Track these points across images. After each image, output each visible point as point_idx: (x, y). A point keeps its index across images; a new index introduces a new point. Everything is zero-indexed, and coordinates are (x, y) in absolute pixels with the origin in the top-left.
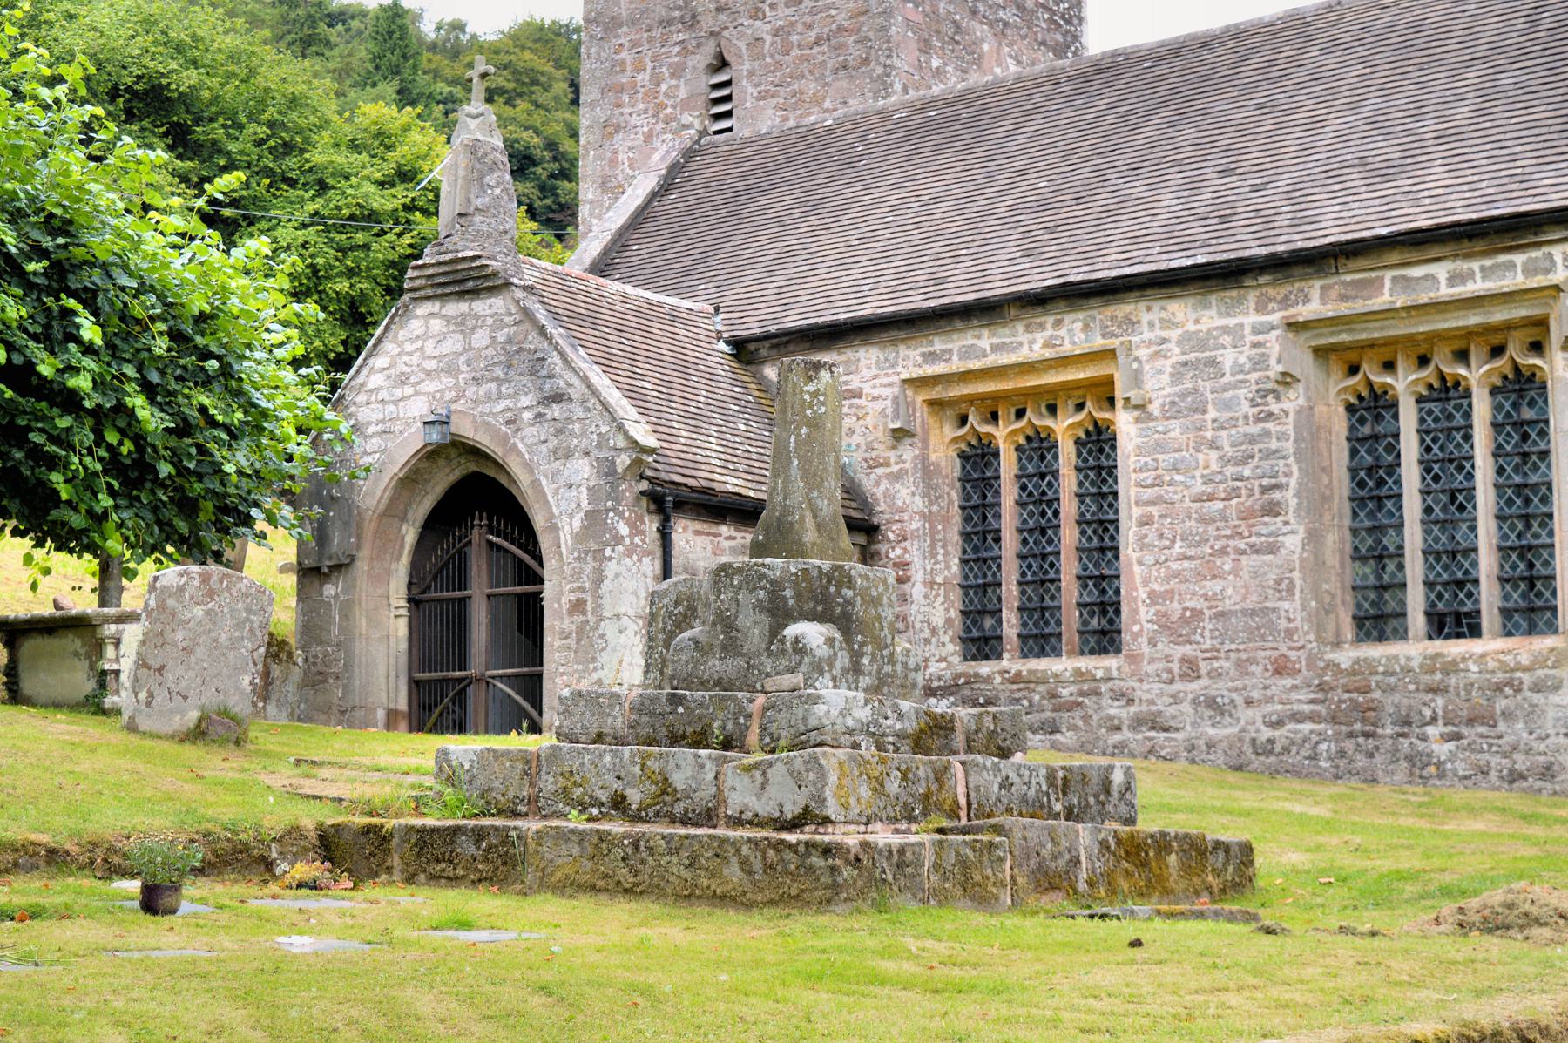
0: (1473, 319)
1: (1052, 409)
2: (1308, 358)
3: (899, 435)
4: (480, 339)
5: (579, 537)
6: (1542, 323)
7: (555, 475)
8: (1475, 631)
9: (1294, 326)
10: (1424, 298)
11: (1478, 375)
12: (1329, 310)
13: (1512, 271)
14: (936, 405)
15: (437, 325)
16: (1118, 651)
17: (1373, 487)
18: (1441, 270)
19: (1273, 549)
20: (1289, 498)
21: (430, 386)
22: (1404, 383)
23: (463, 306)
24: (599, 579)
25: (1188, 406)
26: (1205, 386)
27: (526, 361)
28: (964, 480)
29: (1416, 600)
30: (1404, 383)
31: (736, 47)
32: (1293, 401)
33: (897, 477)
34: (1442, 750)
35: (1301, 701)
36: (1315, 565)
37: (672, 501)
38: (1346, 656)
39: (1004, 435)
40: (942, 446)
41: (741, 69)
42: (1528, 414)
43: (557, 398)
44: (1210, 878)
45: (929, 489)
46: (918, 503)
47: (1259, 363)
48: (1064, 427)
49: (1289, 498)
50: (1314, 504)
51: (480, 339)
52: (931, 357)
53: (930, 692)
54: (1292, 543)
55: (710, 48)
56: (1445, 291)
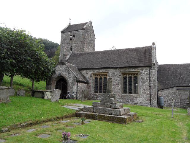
0: (133, 73)
1: (102, 76)
2: (121, 74)
4: (63, 68)
5: (71, 84)
6: (138, 73)
7: (69, 79)
8: (132, 93)
9: (121, 72)
10: (130, 71)
11: (133, 76)
12: (123, 71)
13: (136, 70)
14: (94, 75)
17: (125, 83)
18: (131, 69)
19: (118, 87)
22: (128, 76)
24: (73, 87)
26: (114, 75)
27: (68, 71)
29: (103, 90)
30: (128, 76)
32: (120, 77)
34: (130, 101)
35: (120, 97)
36: (121, 88)
37: (78, 81)
38: (123, 95)
39: (98, 77)
40: (94, 77)
41: (73, 47)
42: (136, 79)
43: (70, 73)
45: (93, 81)
46: (92, 82)
47: (118, 74)
48: (103, 77)
50: (121, 84)
51: (63, 68)
52: (93, 71)
53: (92, 95)
55: (71, 46)
56: (131, 71)
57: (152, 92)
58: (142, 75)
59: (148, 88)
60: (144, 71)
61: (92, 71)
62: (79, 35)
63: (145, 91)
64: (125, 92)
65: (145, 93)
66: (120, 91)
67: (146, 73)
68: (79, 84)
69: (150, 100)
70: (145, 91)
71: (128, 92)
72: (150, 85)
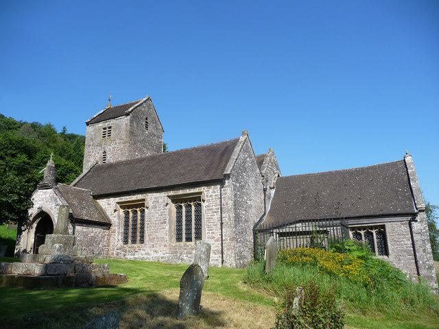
3: (115, 211)
4: (48, 195)
9: (168, 196)
13: (196, 190)
14: (121, 207)
15: (42, 193)
16: (284, 184)
20: (167, 221)
21: (40, 203)
23: (45, 190)
25: (154, 207)
28: (177, 212)
31: (107, 149)
33: (115, 217)
34: (185, 258)
44: (139, 278)
49: (167, 221)
51: (48, 195)
52: (120, 199)
53: (117, 249)
54: (167, 227)
57: (226, 235)
58: (209, 201)
59: (219, 226)
60: (211, 190)
61: (118, 199)
62: (118, 127)
63: (213, 233)
64: (179, 239)
65: (213, 238)
66: (167, 237)
67: (215, 196)
68: (78, 228)
69: (222, 253)
70: (213, 233)
71: (184, 239)
72: (221, 220)
